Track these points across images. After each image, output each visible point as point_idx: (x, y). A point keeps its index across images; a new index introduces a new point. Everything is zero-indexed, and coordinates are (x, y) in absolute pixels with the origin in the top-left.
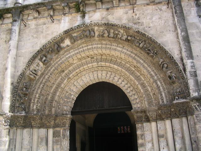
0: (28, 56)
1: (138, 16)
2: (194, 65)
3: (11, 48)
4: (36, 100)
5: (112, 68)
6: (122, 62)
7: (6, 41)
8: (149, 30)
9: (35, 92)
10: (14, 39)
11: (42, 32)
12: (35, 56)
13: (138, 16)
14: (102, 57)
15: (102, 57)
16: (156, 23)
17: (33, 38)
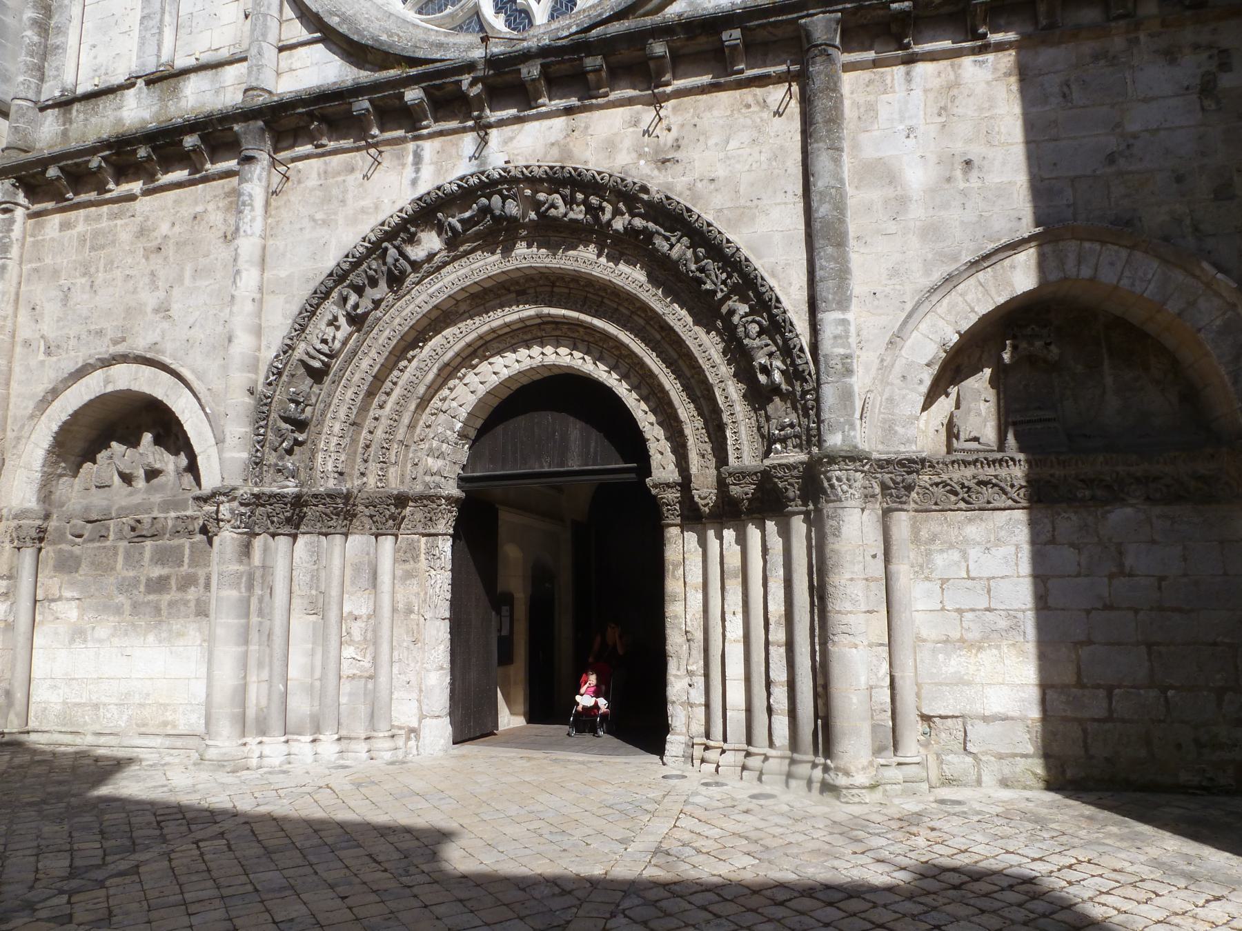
0: (302, 293)
3: (242, 264)
4: (334, 440)
7: (226, 237)
10: (249, 232)
11: (343, 201)
14: (555, 289)
15: (555, 289)
16: (739, 162)
17: (312, 224)
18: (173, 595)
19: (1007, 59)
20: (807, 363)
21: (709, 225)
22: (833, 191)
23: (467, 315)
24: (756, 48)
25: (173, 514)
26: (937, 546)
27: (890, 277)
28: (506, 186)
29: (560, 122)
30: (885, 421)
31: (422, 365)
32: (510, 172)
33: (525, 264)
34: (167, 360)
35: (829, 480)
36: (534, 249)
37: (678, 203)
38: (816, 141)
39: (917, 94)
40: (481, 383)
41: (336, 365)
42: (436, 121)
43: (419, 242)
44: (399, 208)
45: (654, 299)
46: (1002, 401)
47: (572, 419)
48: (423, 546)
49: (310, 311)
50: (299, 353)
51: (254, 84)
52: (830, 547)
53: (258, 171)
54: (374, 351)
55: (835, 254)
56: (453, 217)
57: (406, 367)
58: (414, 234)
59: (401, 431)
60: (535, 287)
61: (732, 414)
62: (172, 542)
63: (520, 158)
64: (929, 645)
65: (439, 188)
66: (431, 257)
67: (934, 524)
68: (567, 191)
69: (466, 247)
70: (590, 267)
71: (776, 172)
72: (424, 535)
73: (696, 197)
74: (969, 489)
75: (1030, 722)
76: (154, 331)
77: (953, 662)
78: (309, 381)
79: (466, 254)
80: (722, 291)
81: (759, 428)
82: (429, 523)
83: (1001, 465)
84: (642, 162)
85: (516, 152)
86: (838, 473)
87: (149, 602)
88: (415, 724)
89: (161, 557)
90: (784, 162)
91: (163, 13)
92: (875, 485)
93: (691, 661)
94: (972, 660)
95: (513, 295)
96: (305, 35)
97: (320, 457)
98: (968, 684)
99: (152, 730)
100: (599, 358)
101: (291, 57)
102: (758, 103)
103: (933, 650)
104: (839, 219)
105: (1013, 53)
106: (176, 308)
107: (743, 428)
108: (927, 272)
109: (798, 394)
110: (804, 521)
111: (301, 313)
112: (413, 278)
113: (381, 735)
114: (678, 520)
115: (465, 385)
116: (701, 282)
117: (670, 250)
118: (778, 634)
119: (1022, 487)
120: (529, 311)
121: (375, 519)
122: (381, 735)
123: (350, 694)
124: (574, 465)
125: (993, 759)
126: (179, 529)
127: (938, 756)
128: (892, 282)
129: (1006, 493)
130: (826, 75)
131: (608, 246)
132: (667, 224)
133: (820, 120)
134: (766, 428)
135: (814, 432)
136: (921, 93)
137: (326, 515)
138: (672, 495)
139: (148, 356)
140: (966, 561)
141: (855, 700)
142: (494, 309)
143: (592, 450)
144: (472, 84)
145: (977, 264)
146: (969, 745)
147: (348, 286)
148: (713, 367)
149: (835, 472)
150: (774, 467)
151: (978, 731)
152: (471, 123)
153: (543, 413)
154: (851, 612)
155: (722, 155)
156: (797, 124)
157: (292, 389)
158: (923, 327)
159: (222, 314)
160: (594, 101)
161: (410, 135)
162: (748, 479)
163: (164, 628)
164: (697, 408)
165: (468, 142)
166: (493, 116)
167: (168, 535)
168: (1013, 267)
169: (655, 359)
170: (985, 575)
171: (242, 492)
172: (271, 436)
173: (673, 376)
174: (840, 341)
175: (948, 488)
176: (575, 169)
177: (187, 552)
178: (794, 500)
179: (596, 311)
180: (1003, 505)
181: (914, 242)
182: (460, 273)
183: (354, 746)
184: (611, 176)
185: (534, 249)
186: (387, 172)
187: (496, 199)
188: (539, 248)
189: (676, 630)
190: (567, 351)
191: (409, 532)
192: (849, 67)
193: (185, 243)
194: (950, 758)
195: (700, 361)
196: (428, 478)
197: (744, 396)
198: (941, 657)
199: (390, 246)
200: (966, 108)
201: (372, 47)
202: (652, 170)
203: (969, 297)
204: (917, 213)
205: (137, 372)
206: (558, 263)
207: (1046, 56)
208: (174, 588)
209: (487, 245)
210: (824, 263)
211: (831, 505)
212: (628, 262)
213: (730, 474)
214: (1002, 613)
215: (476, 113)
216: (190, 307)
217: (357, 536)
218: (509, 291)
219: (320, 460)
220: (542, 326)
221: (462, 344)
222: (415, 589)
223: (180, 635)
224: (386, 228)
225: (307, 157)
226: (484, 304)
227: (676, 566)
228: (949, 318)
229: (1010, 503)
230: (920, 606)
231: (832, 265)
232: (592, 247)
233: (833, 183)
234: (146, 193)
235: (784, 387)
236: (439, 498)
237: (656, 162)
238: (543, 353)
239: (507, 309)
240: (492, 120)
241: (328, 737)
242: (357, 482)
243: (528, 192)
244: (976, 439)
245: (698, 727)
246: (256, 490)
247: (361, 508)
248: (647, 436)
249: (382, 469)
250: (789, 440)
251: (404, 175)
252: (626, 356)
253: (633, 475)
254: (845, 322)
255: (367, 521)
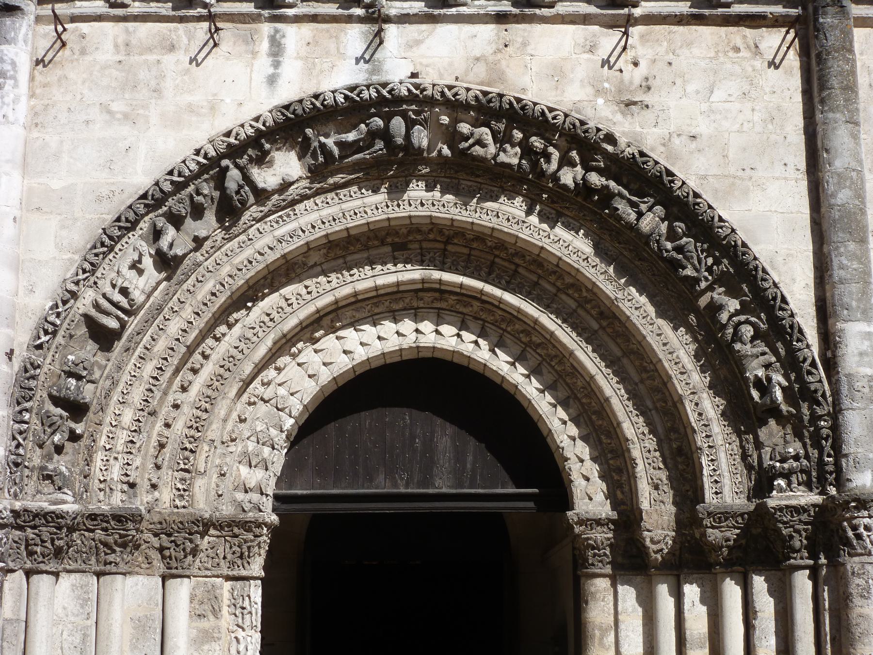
1: (643, 68)
4: (123, 436)
5: (487, 306)
8: (691, 153)
9: (116, 397)
10: (11, 118)
11: (157, 91)
13: (643, 68)
16: (726, 118)
20: (820, 381)
21: (696, 195)
22: (854, 174)
23: (319, 269)
28: (414, 107)
32: (424, 90)
33: (506, 227)
35: (855, 528)
36: (437, 194)
37: (656, 163)
38: (831, 110)
40: (324, 364)
41: (133, 324)
43: (271, 164)
44: (254, 115)
47: (439, 421)
48: (226, 595)
52: (857, 611)
53: (24, 30)
55: (858, 252)
56: (327, 136)
57: (224, 335)
58: (268, 153)
59: (214, 426)
60: (420, 241)
61: (707, 436)
63: (429, 69)
65: (316, 96)
66: (285, 186)
68: (502, 126)
69: (338, 179)
70: (515, 227)
71: (773, 137)
72: (228, 578)
73: (672, 156)
78: (92, 346)
79: (337, 187)
80: (706, 279)
81: (744, 456)
82: (239, 562)
84: (600, 101)
85: (424, 61)
86: (867, 521)
90: (782, 127)
95: (388, 249)
100: (497, 344)
102: (748, 47)
104: (861, 209)
109: (806, 418)
110: (810, 578)
111: (94, 247)
112: (254, 211)
114: (608, 570)
115: (299, 365)
116: (677, 265)
117: (638, 220)
120: (412, 273)
124: (443, 486)
130: (842, 32)
131: (541, 202)
132: (633, 186)
133: (836, 86)
134: (755, 456)
138: (602, 536)
142: (359, 265)
143: (469, 466)
147: (163, 215)
148: (682, 373)
150: (781, 509)
153: (396, 410)
155: (704, 107)
156: (796, 82)
157: (71, 357)
161: (266, 13)
162: (731, 522)
164: (649, 423)
169: (591, 354)
172: (36, 424)
173: (615, 379)
174: (866, 359)
179: (508, 283)
185: (437, 194)
187: (398, 124)
190: (454, 330)
191: (209, 573)
195: (666, 364)
196: (240, 496)
197: (723, 414)
199: (231, 166)
202: (614, 113)
206: (470, 216)
209: (367, 180)
210: (845, 262)
211: (856, 559)
212: (568, 226)
213: (709, 514)
217: (140, 578)
218: (383, 243)
220: (421, 294)
224: (232, 140)
226: (344, 257)
227: (604, 631)
232: (519, 200)
233: (853, 164)
235: (784, 408)
236: (259, 525)
238: (417, 331)
239: (379, 267)
240: (393, 12)
243: (445, 119)
246: (18, 505)
248: (568, 453)
249: (183, 480)
250: (794, 476)
251: (256, 67)
253: (531, 504)
255: (155, 556)
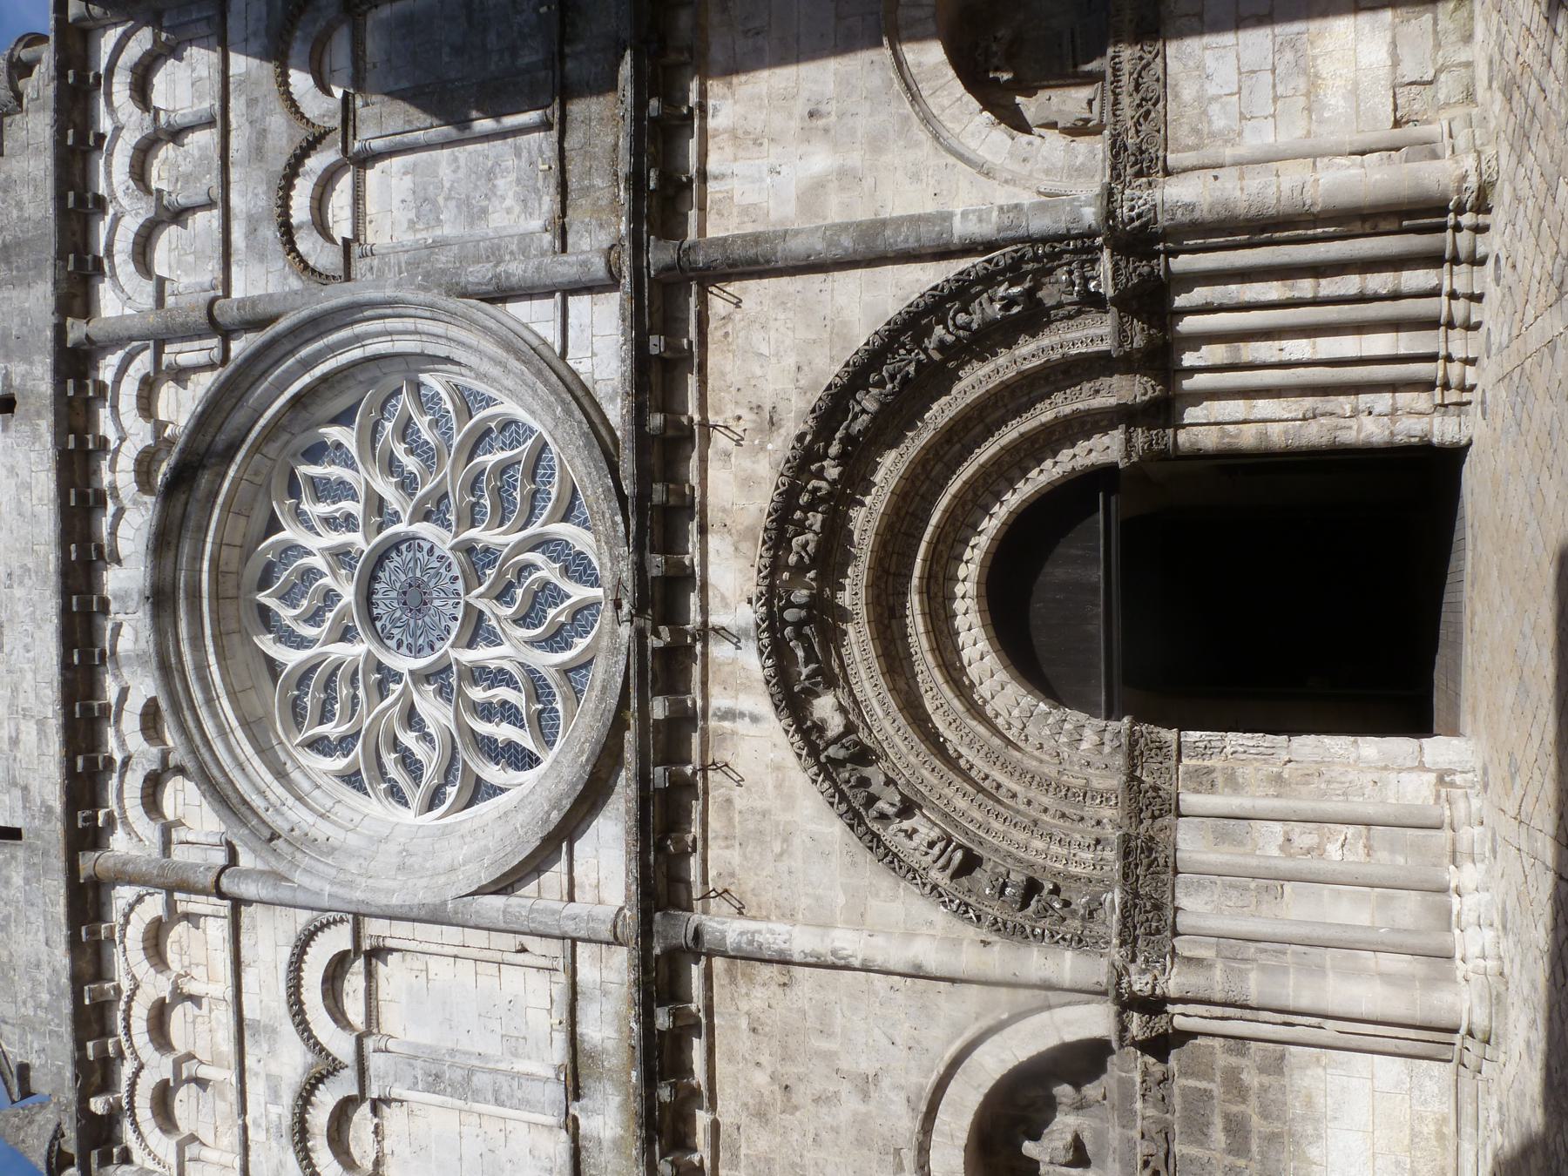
0: (869, 868)
2: (974, 211)
4: (1055, 848)
6: (921, 492)
7: (785, 984)
10: (787, 937)
12: (871, 841)
16: (783, 342)
17: (785, 857)
18: (1251, 1109)
19: (715, 87)
20: (1004, 255)
21: (847, 365)
22: (828, 233)
24: (670, 323)
25: (1139, 1105)
26: (1204, 127)
27: (919, 180)
29: (713, 541)
30: (1070, 176)
31: (967, 740)
32: (761, 593)
34: (933, 1078)
35: (1132, 220)
36: (847, 581)
37: (820, 399)
39: (738, 167)
41: (959, 838)
42: (688, 692)
43: (823, 721)
44: (784, 734)
45: (917, 441)
46: (1052, 83)
47: (1041, 578)
48: (1194, 762)
49: (891, 859)
50: (941, 878)
51: (609, 926)
52: (1205, 214)
54: (946, 791)
56: (800, 674)
57: (968, 761)
59: (1046, 771)
62: (1177, 1108)
64: (1314, 127)
66: (842, 709)
67: (1180, 132)
68: (791, 528)
69: (835, 664)
71: (798, 302)
72: (1179, 760)
74: (1143, 99)
75: (1397, 20)
76: (892, 1102)
77: (1332, 102)
78: (977, 874)
79: (842, 666)
80: (918, 354)
81: (1070, 317)
82: (1165, 750)
83: (1119, 70)
84: (770, 446)
85: (739, 592)
86: (1125, 210)
87: (1262, 1153)
88: (1432, 777)
89: (1198, 1130)
90: (789, 295)
91: (497, 1071)
92: (1138, 183)
93: (1340, 411)
94: (1330, 82)
96: (561, 866)
97: (1074, 869)
98: (1356, 84)
99: (1451, 1160)
101: (582, 886)
103: (1320, 122)
105: (710, 82)
106: (866, 1065)
107: (1068, 336)
108: (918, 144)
112: (862, 735)
113: (1447, 813)
114: (1170, 432)
116: (906, 380)
118: (1305, 287)
119: (1142, 49)
120: (914, 602)
121: (1157, 813)
122: (1447, 813)
123: (1392, 851)
125: (1440, 53)
126: (1160, 1097)
127: (1440, 108)
128: (925, 178)
129: (1148, 64)
130: (710, 247)
131: (854, 494)
134: (1070, 308)
135: (1079, 243)
136: (738, 164)
137: (1150, 866)
138: (1140, 437)
139: (924, 1109)
140: (1220, 97)
141: (1378, 176)
142: (907, 647)
143: (1080, 553)
144: (658, 636)
145: (913, 94)
146: (1426, 78)
149: (1124, 212)
150: (1116, 285)
151: (1409, 71)
152: (698, 647)
154: (1278, 187)
155: (774, 360)
156: (752, 284)
157: (987, 892)
158: (973, 144)
159: (882, 993)
160: (697, 500)
161: (700, 723)
163: (1299, 1129)
164: (1041, 399)
165: (720, 651)
166: (695, 617)
167: (1168, 1116)
168: (919, 65)
170: (1236, 77)
171: (1117, 957)
173: (1004, 428)
174: (984, 216)
175: (1141, 120)
176: (770, 514)
177: (1192, 1083)
178: (1152, 268)
179: (922, 521)
180: (1162, 65)
181: (886, 158)
182: (864, 676)
183: (1463, 846)
184: (782, 475)
185: (847, 581)
186: (738, 755)
188: (846, 576)
189: (1302, 432)
190: (963, 566)
192: (702, 230)
193: (785, 1047)
194: (1442, 97)
195: (991, 386)
196: (1107, 749)
198: (1326, 115)
200: (757, 121)
201: (595, 766)
202: (779, 435)
203: (946, 102)
204: (855, 158)
205: (943, 1134)
207: (717, 53)
208: (1242, 1107)
211: (1159, 218)
212: (874, 471)
213: (1121, 346)
214: (1277, 57)
215: (689, 640)
216: (866, 1044)
217: (1179, 836)
218: (889, 627)
219: (1079, 870)
221: (945, 687)
222: (1250, 770)
223: (1309, 1103)
224: (804, 753)
225: (705, 861)
227: (1225, 434)
228: (965, 121)
229: (1159, 60)
230: (1271, 140)
231: (904, 229)
234: (713, 1106)
235: (1027, 285)
237: (771, 431)
238: (963, 597)
240: (699, 619)
241: (1453, 877)
242: (1109, 828)
243: (786, 575)
244: (1090, 103)
245: (1420, 400)
246: (1115, 941)
247: (1142, 829)
248: (1069, 467)
249: (1093, 798)
252: (975, 494)
253: (1113, 499)
254: (964, 214)
255: (1159, 823)
